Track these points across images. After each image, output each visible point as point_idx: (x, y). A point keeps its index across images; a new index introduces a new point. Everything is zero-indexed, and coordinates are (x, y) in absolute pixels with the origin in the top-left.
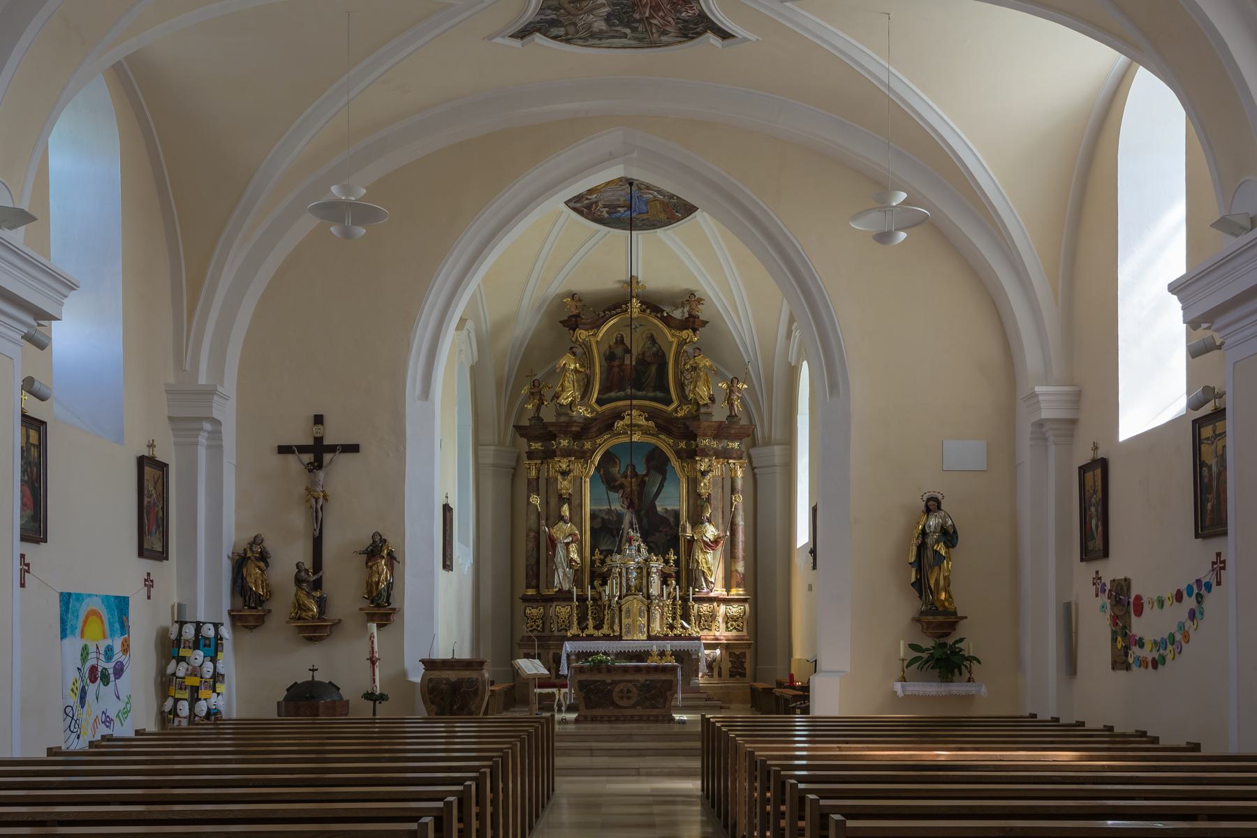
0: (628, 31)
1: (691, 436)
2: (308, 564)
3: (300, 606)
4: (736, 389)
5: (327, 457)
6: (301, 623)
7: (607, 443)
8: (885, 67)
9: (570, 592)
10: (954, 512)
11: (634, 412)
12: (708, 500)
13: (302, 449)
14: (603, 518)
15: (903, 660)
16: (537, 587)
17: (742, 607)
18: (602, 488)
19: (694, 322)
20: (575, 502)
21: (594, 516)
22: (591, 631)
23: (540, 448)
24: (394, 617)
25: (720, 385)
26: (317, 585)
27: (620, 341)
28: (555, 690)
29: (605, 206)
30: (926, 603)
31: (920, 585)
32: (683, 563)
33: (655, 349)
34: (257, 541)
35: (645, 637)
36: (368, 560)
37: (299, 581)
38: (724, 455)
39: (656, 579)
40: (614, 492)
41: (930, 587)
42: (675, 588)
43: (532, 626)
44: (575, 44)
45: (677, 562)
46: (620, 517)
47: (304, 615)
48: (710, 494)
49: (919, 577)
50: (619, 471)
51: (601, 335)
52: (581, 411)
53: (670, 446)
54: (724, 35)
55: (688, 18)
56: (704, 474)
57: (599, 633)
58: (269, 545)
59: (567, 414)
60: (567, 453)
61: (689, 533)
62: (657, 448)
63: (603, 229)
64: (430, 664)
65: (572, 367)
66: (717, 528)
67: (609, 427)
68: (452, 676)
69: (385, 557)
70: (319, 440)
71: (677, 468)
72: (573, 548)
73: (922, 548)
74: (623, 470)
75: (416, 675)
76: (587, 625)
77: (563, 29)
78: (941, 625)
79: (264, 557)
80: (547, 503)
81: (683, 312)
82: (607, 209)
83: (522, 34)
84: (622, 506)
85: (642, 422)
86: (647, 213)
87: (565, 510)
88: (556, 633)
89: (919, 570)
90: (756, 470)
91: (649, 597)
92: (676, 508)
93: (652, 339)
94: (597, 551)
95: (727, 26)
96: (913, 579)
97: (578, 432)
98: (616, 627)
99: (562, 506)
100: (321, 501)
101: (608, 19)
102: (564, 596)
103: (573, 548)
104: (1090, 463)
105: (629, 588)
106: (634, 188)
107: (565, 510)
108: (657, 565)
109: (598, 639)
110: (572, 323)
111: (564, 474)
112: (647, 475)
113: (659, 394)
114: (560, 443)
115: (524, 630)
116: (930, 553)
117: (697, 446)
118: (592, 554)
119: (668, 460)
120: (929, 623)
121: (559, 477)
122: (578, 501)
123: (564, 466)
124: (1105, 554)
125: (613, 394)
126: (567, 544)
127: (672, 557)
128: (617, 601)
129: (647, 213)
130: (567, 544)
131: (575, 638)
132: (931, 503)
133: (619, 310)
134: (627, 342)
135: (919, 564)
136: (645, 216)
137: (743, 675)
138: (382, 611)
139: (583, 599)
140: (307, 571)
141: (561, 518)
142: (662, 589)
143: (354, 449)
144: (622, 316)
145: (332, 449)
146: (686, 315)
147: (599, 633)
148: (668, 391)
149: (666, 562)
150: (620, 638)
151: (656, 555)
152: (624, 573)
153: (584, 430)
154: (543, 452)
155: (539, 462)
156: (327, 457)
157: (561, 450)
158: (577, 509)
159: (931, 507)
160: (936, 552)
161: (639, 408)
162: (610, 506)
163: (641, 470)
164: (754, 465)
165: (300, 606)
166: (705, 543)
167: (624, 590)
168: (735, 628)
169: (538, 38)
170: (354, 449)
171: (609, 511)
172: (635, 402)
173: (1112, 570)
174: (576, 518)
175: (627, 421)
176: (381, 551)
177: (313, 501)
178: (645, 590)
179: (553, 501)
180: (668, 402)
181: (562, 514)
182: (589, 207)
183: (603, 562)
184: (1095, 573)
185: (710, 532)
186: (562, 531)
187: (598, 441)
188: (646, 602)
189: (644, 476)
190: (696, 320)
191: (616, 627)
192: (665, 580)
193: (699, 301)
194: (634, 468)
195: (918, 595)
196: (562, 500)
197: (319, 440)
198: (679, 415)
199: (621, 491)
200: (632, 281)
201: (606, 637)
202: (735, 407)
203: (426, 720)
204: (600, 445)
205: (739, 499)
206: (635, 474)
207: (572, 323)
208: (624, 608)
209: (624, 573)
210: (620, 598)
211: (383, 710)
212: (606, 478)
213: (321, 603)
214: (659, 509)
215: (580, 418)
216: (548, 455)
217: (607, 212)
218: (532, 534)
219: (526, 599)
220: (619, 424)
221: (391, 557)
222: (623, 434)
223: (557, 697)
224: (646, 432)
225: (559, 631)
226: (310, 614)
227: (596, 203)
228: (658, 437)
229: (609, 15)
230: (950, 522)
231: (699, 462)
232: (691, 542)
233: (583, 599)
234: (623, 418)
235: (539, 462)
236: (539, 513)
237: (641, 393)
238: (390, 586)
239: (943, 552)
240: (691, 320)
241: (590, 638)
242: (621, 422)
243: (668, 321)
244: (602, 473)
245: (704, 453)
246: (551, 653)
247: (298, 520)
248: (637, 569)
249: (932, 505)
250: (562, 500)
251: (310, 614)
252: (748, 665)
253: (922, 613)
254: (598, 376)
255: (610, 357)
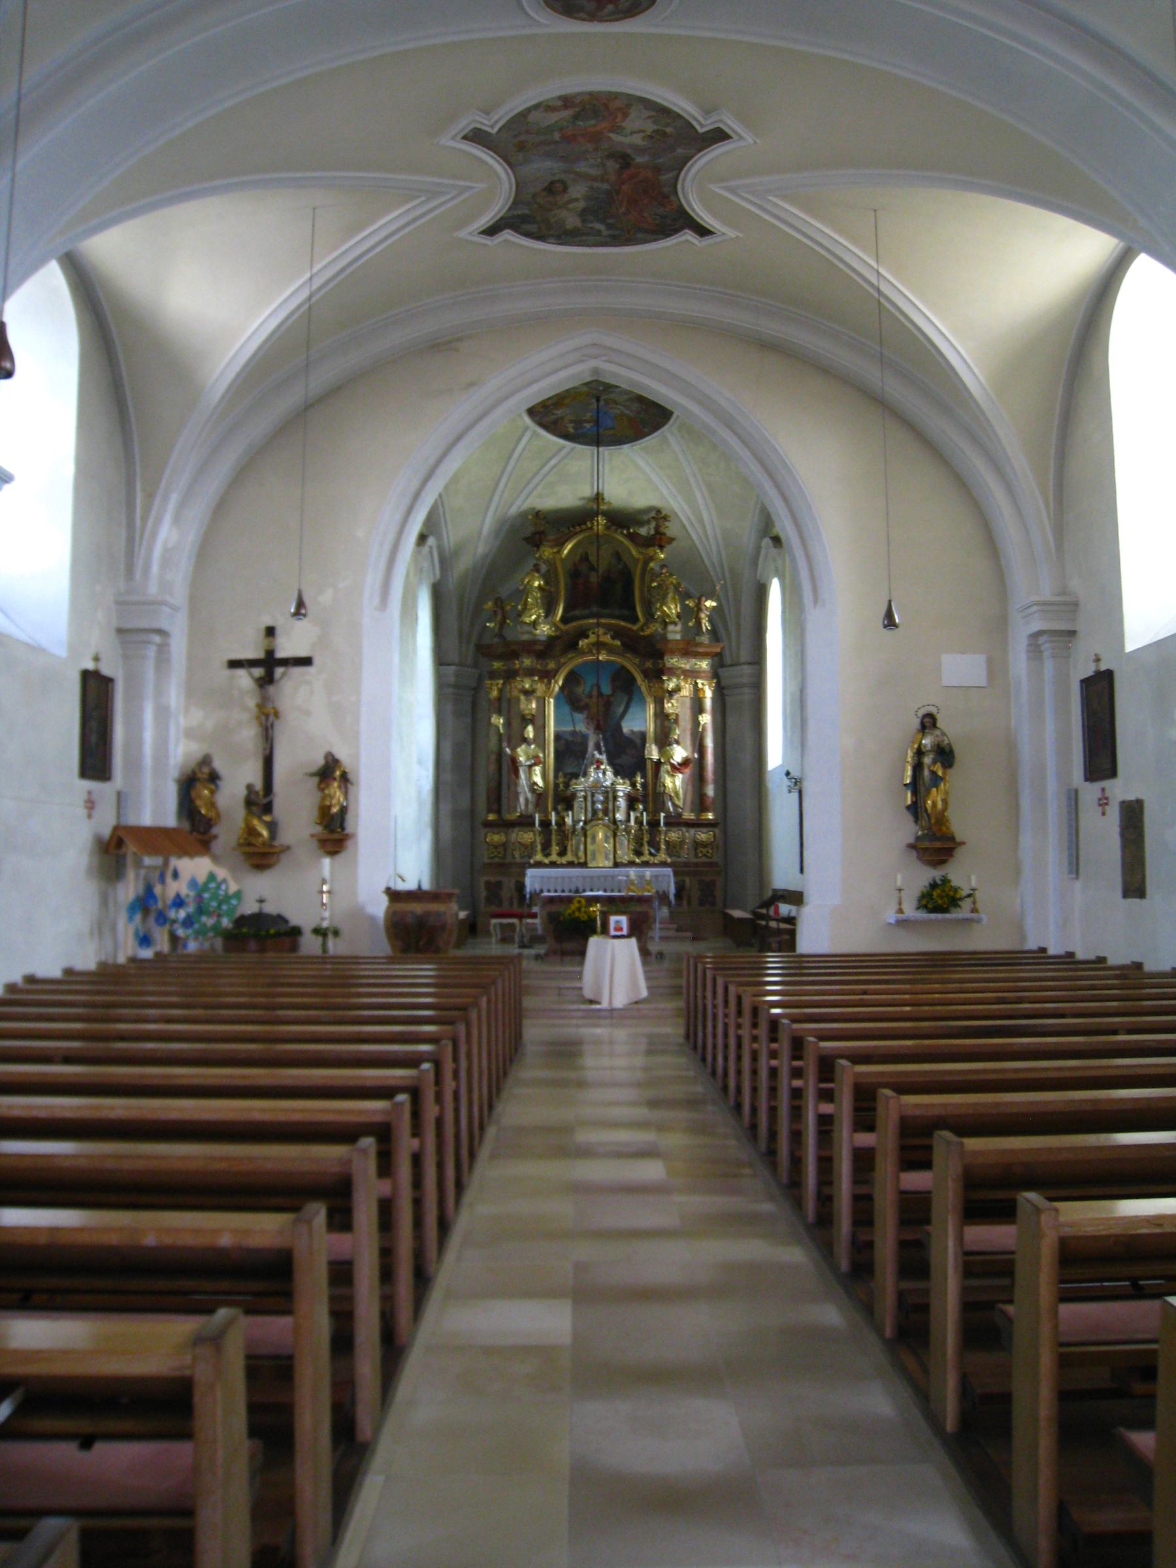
0: (601, 227)
1: (659, 655)
2: (259, 785)
3: (251, 832)
4: (703, 608)
5: (279, 671)
6: (248, 849)
7: (574, 662)
8: (874, 268)
9: (532, 817)
10: (951, 728)
11: (601, 631)
12: (676, 721)
13: (252, 663)
14: (566, 740)
15: (900, 890)
16: (499, 812)
17: (711, 833)
18: (567, 709)
19: (661, 539)
20: (539, 723)
21: (558, 737)
22: (554, 857)
23: (502, 668)
24: (349, 843)
25: (687, 602)
26: (268, 808)
27: (585, 558)
28: (515, 921)
29: (571, 421)
30: (922, 828)
31: (915, 809)
32: (650, 788)
33: (620, 567)
34: (206, 761)
35: (611, 864)
36: (321, 782)
37: (249, 803)
38: (692, 674)
39: (622, 803)
40: (579, 713)
41: (926, 811)
42: (642, 814)
43: (493, 853)
44: (548, 243)
45: (644, 785)
46: (585, 738)
47: (253, 840)
48: (677, 715)
49: (914, 800)
50: (584, 691)
51: (566, 552)
52: (544, 629)
53: (637, 665)
54: (703, 231)
55: (665, 213)
56: (671, 693)
57: (564, 860)
58: (218, 764)
59: (531, 633)
60: (530, 673)
61: (655, 755)
62: (623, 668)
63: (569, 445)
64: (395, 896)
65: (536, 584)
66: (685, 748)
67: (572, 646)
68: (418, 908)
69: (338, 779)
70: (270, 653)
71: (643, 688)
72: (537, 770)
73: (918, 767)
74: (588, 689)
75: (379, 907)
76: (550, 851)
77: (536, 226)
78: (939, 851)
79: (214, 778)
80: (508, 724)
81: (649, 529)
82: (573, 425)
83: (492, 231)
84: (587, 728)
85: (607, 639)
86: (613, 428)
87: (530, 732)
88: (518, 860)
89: (915, 793)
90: (725, 692)
91: (615, 822)
92: (642, 729)
93: (618, 556)
94: (561, 774)
95: (706, 222)
96: (909, 802)
97: (541, 650)
98: (581, 854)
99: (525, 727)
100: (272, 718)
101: (584, 214)
102: (525, 822)
103: (537, 770)
104: (1092, 676)
105: (595, 812)
106: (602, 403)
107: (530, 732)
108: (623, 788)
109: (562, 866)
110: (535, 540)
111: (528, 693)
112: (612, 695)
113: (625, 612)
114: (523, 662)
115: (484, 857)
116: (926, 773)
117: (664, 666)
118: (556, 777)
119: (634, 680)
120: (926, 850)
121: (522, 697)
122: (542, 722)
123: (527, 686)
124: (1113, 773)
125: (577, 612)
126: (530, 767)
127: (639, 779)
128: (582, 827)
129: (613, 428)
130: (530, 767)
131: (539, 865)
132: (927, 720)
133: (584, 527)
134: (593, 559)
135: (915, 786)
136: (612, 432)
137: (713, 904)
138: (336, 836)
139: (546, 824)
140: (257, 793)
141: (525, 740)
142: (629, 815)
143: (306, 661)
144: (587, 534)
145: (286, 662)
146: (652, 532)
147: (564, 860)
148: (634, 609)
149: (633, 785)
150: (584, 865)
151: (622, 778)
152: (589, 798)
153: (546, 650)
154: (505, 671)
155: (501, 682)
156: (279, 671)
157: (524, 669)
158: (541, 729)
159: (927, 724)
160: (933, 773)
161: (608, 628)
162: (575, 727)
163: (606, 689)
164: (723, 683)
165: (251, 832)
166: (673, 766)
167: (589, 815)
168: (705, 855)
169: (507, 235)
170: (306, 661)
171: (574, 733)
172: (603, 621)
173: (1120, 789)
174: (540, 740)
175: (592, 638)
176: (333, 772)
177: (263, 718)
178: (611, 815)
179: (516, 723)
180: (635, 620)
181: (526, 736)
182: (555, 422)
183: (567, 785)
184: (1100, 791)
185: (679, 753)
186: (522, 755)
187: (562, 660)
188: (612, 827)
189: (609, 696)
190: (663, 537)
191: (581, 854)
192: (631, 806)
193: (665, 518)
194: (599, 687)
195: (914, 819)
196: (526, 720)
197: (270, 653)
198: (646, 633)
199: (586, 712)
200: (598, 497)
201: (571, 864)
202: (703, 625)
203: (391, 960)
204: (564, 664)
205: (706, 719)
206: (600, 694)
207: (535, 540)
208: (589, 833)
209: (589, 798)
210: (586, 823)
211: (335, 947)
212: (570, 699)
213: (272, 827)
214: (625, 730)
215: (543, 636)
216: (510, 675)
217: (573, 428)
218: (493, 757)
219: (488, 825)
220: (582, 643)
221: (345, 779)
222: (587, 652)
223: (518, 929)
224: (611, 650)
225: (522, 857)
226: (260, 840)
227: (562, 418)
228: (624, 656)
229: (584, 210)
230: (946, 739)
231: (666, 682)
232: (658, 764)
233: (546, 824)
234: (587, 637)
235: (501, 682)
236: (500, 735)
237: (606, 611)
238: (344, 810)
239: (940, 773)
240: (658, 536)
241: (553, 864)
242: (586, 641)
243: (633, 537)
244: (566, 693)
245: (672, 672)
246: (513, 881)
247: (249, 735)
248: (605, 793)
249: (928, 722)
250: (526, 720)
251: (260, 840)
252: (718, 893)
253: (918, 838)
254: (563, 593)
255: (575, 574)
